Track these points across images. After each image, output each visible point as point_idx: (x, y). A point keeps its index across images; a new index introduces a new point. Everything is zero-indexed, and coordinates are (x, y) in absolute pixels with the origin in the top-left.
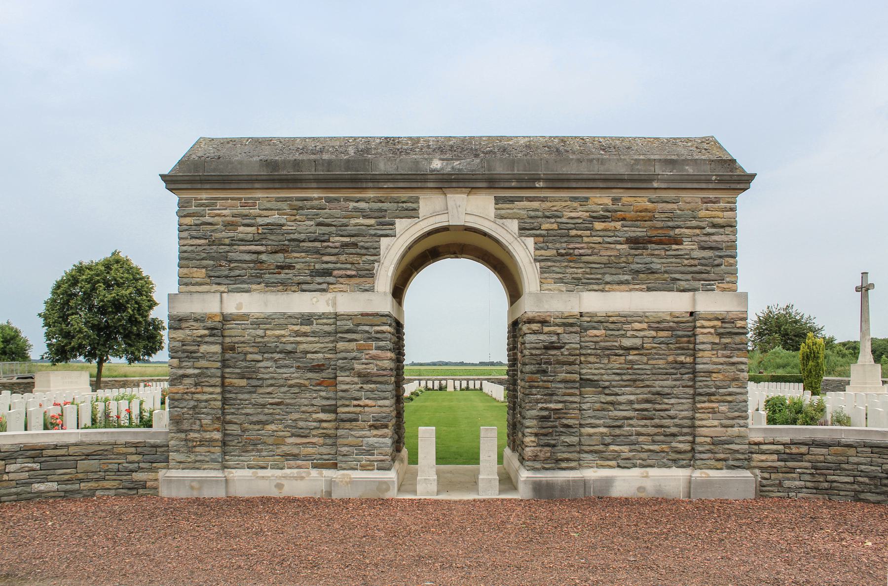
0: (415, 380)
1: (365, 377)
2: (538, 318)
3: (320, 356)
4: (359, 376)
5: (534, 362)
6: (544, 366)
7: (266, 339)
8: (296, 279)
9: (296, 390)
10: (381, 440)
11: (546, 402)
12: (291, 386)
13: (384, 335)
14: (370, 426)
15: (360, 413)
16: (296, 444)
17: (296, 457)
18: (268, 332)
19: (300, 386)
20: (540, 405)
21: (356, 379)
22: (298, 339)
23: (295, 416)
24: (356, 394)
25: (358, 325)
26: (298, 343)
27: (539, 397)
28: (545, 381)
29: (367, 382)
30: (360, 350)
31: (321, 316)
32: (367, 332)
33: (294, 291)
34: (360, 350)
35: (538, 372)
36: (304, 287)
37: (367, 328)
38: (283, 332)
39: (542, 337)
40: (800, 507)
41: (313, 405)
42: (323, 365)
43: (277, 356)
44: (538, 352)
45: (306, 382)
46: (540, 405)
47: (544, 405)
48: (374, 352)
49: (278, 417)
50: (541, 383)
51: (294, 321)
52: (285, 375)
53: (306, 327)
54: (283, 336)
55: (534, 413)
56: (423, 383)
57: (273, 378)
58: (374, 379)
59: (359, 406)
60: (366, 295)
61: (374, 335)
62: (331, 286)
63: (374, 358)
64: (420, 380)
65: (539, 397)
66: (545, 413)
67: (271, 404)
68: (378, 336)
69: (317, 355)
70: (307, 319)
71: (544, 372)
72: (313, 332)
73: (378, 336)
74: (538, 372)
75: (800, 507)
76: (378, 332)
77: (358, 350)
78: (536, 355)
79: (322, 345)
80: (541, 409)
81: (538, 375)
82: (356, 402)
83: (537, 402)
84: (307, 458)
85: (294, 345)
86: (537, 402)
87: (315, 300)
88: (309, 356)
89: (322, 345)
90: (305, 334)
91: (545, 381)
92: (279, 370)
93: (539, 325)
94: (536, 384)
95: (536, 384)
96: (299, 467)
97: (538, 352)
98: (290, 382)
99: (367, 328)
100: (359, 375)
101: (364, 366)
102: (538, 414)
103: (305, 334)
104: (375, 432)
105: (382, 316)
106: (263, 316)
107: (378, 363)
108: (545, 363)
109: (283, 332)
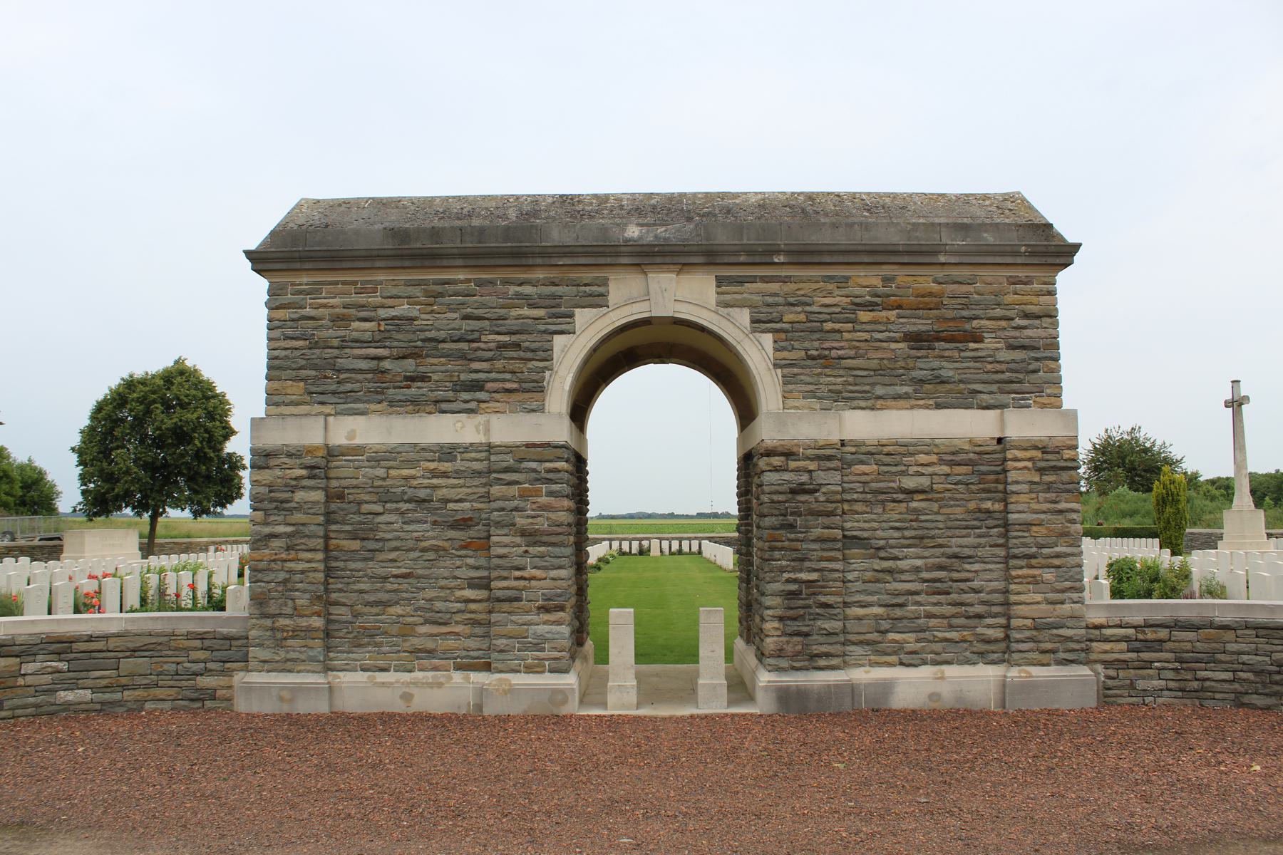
0: (604, 539)
1: (532, 537)
2: (780, 449)
3: (467, 505)
7: (389, 482)
8: (433, 395)
9: (432, 555)
11: (794, 570)
12: (424, 550)
13: (560, 475)
14: (539, 608)
17: (430, 653)
18: (392, 472)
19: (436, 549)
20: (786, 575)
21: (518, 540)
22: (435, 481)
23: (430, 594)
24: (518, 561)
25: (521, 460)
27: (784, 563)
28: (792, 540)
29: (535, 544)
32: (534, 471)
33: (430, 413)
35: (782, 527)
36: (444, 406)
38: (412, 472)
39: (787, 476)
41: (456, 578)
42: (470, 519)
44: (781, 498)
45: (446, 544)
46: (786, 575)
47: (792, 575)
48: (544, 500)
50: (786, 543)
53: (446, 464)
54: (414, 477)
55: (777, 586)
56: (616, 544)
57: (398, 538)
58: (545, 539)
61: (543, 475)
63: (544, 508)
64: (611, 540)
65: (784, 563)
66: (794, 587)
67: (396, 576)
68: (550, 476)
70: (448, 452)
71: (791, 527)
72: (457, 472)
73: (550, 476)
74: (782, 527)
76: (549, 471)
79: (469, 490)
80: (788, 581)
82: (518, 574)
84: (447, 654)
85: (428, 490)
86: (782, 570)
87: (459, 425)
88: (450, 506)
89: (469, 490)
90: (445, 475)
91: (792, 540)
92: (407, 527)
93: (782, 458)
94: (779, 544)
95: (779, 544)
96: (435, 669)
97: (781, 498)
99: (533, 465)
100: (523, 533)
101: (530, 520)
102: (783, 588)
104: (546, 617)
106: (384, 448)
109: (412, 472)
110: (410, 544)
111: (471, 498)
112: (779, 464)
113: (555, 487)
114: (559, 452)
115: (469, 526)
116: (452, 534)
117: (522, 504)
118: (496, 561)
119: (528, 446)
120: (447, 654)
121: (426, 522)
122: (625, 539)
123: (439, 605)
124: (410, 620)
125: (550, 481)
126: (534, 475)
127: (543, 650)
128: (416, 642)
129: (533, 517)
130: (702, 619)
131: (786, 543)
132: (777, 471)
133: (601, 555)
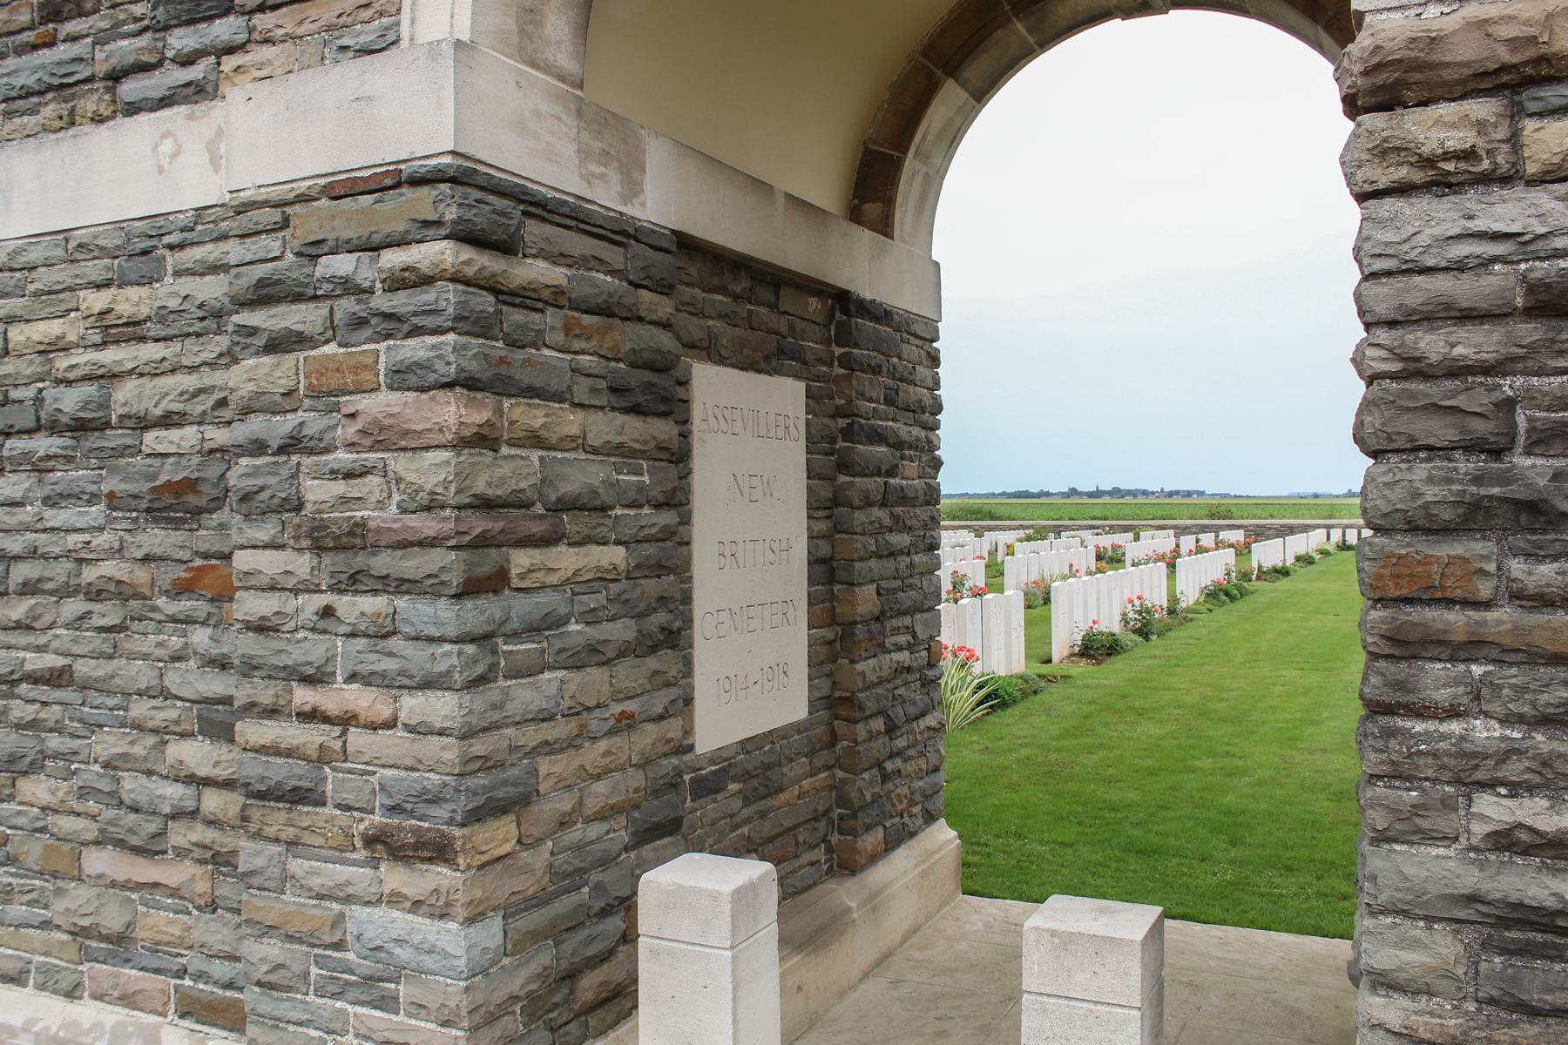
0: (1318, 527)
1: (342, 545)
2: (1467, 52)
3: (187, 436)
4: (318, 548)
5: (1440, 431)
9: (108, 613)
10: (424, 928)
12: (96, 594)
13: (427, 296)
14: (370, 841)
15: (323, 757)
16: (126, 886)
17: (120, 944)
19: (122, 592)
20: (1494, 810)
21: (302, 564)
22: (110, 356)
23: (109, 743)
24: (309, 650)
25: (312, 251)
26: (113, 376)
27: (1485, 732)
29: (353, 582)
30: (325, 395)
31: (200, 224)
32: (348, 287)
33: (98, 120)
34: (325, 395)
35: (1473, 517)
36: (130, 89)
37: (341, 265)
38: (54, 328)
39: (1507, 211)
41: (166, 695)
42: (190, 485)
43: (43, 444)
44: (1472, 343)
45: (142, 575)
46: (1494, 810)
48: (380, 404)
49: (54, 742)
50: (1502, 618)
51: (94, 269)
52: (73, 540)
53: (134, 293)
54: (58, 346)
55: (1435, 867)
56: (1336, 535)
57: (33, 554)
58: (383, 562)
59: (312, 716)
60: (352, 75)
61: (381, 301)
62: (229, 63)
63: (382, 437)
64: (1328, 527)
65: (1485, 732)
67: (34, 679)
68: (402, 302)
69: (174, 434)
70: (143, 248)
72: (163, 315)
73: (402, 302)
74: (1473, 517)
76: (399, 282)
77: (315, 393)
78: (1457, 371)
79: (189, 382)
80: (1506, 841)
81: (1476, 548)
82: (304, 696)
83: (1472, 774)
84: (163, 958)
85: (90, 389)
86: (1472, 774)
87: (167, 147)
88: (151, 439)
89: (189, 382)
92: (55, 517)
93: (1483, 108)
94: (1455, 620)
95: (1455, 620)
96: (128, 1000)
97: (1472, 343)
98: (90, 574)
99: (341, 265)
100: (321, 540)
101: (340, 487)
102: (1470, 879)
104: (395, 877)
105: (417, 181)
107: (399, 464)
109: (54, 328)
110: (59, 572)
111: (197, 408)
112: (1458, 139)
113: (415, 349)
114: (422, 201)
115: (197, 512)
116: (157, 539)
117: (312, 422)
119: (342, 189)
120: (163, 958)
121: (93, 499)
122: (1351, 526)
124: (66, 824)
125: (394, 325)
126: (347, 306)
128: (76, 901)
129: (349, 475)
131: (1502, 618)
132: (1443, 185)
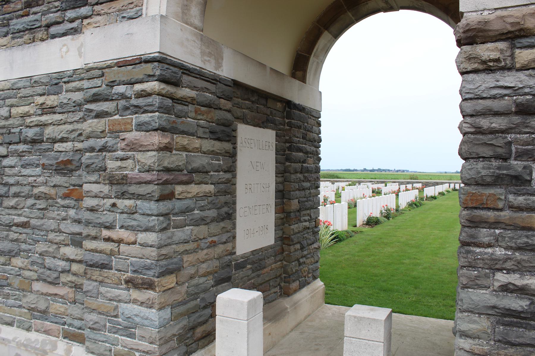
0: (446, 183)
1: (119, 183)
2: (497, 26)
3: (68, 145)
4: (111, 184)
5: (487, 152)
6: (517, 165)
7: (11, 121)
8: (45, 20)
9: (41, 204)
10: (144, 311)
11: (520, 269)
13: (149, 100)
14: (127, 282)
15: (112, 253)
16: (47, 294)
17: (44, 314)
18: (14, 111)
19: (46, 197)
20: (502, 278)
21: (106, 189)
23: (41, 247)
24: (107, 217)
25: (111, 84)
26: (45, 125)
27: (499, 252)
28: (519, 209)
29: (122, 195)
30: (115, 132)
32: (123, 96)
33: (42, 40)
34: (115, 132)
35: (497, 181)
36: (53, 30)
37: (121, 89)
38: (26, 109)
39: (510, 79)
40: (74, 106)
41: (60, 231)
42: (69, 162)
43: (22, 147)
44: (497, 123)
45: (53, 192)
46: (502, 278)
47: (515, 279)
48: (133, 136)
50: (506, 214)
51: (39, 89)
52: (31, 179)
53: (52, 97)
55: (483, 297)
56: (452, 186)
58: (133, 189)
61: (134, 101)
62: (86, 22)
64: (450, 183)
65: (499, 252)
66: (519, 304)
67: (17, 225)
68: (141, 102)
70: (56, 82)
71: (519, 181)
72: (62, 105)
73: (141, 102)
75: (74, 106)
77: (111, 132)
78: (493, 132)
80: (506, 288)
81: (498, 191)
82: (106, 233)
85: (37, 129)
86: (495, 266)
87: (64, 49)
90: (51, 110)
91: (519, 209)
92: (25, 172)
93: (502, 45)
94: (491, 215)
95: (491, 215)
96: (47, 332)
97: (497, 123)
98: (36, 191)
99: (121, 89)
100: (112, 181)
101: (119, 163)
102: (493, 301)
103: (51, 110)
104: (135, 294)
105: (147, 61)
106: (8, 85)
108: (520, 156)
109: (26, 109)
111: (72, 136)
112: (494, 55)
113: (145, 117)
116: (58, 179)
118: (87, 215)
119: (122, 64)
121: (37, 166)
123: (48, 261)
124: (27, 273)
125: (138, 109)
127: (132, 336)
128: (30, 299)
129: (122, 159)
130: (349, 330)
131: (506, 214)
132: (489, 70)
133: (441, 191)
